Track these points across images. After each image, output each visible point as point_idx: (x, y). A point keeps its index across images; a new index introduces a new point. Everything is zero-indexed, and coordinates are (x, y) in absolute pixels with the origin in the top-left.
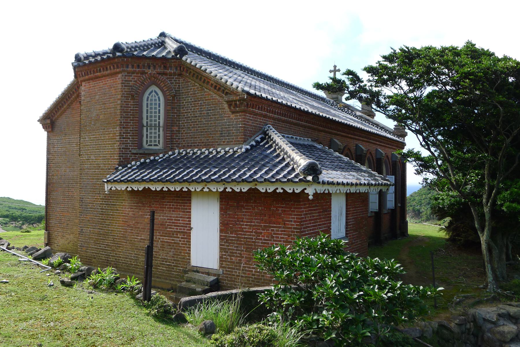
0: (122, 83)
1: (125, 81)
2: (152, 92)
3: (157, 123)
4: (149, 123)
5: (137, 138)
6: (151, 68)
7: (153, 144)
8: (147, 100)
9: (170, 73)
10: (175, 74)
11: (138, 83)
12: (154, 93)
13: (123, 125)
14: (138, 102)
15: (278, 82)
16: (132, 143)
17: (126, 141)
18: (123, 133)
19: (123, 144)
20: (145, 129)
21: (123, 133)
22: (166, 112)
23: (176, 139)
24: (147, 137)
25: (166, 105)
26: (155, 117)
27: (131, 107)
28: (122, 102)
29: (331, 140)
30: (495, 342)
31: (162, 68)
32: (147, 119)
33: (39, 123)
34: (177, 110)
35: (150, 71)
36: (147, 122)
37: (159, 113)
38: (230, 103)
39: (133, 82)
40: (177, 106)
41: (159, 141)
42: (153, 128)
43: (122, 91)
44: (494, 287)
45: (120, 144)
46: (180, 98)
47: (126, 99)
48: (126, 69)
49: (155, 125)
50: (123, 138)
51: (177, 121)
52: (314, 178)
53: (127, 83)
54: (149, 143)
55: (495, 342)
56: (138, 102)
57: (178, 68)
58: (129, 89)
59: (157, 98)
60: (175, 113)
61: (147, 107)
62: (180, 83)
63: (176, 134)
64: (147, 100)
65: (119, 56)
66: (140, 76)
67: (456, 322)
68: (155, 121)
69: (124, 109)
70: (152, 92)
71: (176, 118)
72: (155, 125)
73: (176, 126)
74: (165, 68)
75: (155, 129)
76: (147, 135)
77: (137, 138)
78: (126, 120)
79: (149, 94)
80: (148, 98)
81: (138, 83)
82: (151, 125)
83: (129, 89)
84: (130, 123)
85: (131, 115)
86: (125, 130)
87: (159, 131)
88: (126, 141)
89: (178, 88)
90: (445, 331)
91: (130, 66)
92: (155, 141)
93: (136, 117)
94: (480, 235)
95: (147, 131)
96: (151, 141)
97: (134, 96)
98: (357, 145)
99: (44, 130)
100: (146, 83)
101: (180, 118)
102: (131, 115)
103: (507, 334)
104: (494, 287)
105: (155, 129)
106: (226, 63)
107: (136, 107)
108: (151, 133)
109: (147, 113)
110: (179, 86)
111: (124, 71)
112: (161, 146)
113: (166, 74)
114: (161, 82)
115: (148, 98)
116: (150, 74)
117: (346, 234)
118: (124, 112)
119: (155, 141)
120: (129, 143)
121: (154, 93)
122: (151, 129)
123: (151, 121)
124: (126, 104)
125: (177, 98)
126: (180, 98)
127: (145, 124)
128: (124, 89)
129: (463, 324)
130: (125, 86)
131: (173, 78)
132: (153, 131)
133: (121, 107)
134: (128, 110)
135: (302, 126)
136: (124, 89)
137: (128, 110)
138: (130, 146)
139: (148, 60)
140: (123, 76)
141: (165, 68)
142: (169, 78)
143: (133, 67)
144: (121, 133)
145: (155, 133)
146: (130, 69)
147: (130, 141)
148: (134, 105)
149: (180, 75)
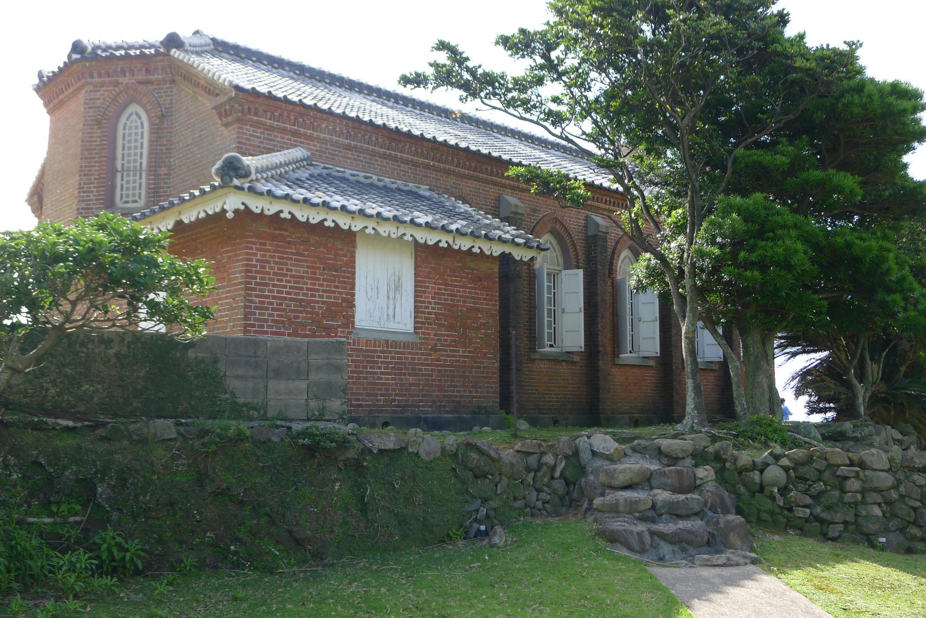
0: (85, 104)
1: (90, 99)
2: (131, 114)
3: (138, 165)
4: (126, 165)
5: (103, 191)
6: (127, 74)
7: (131, 199)
8: (124, 129)
9: (157, 80)
10: (164, 80)
11: (108, 101)
12: (134, 117)
13: (85, 171)
14: (107, 132)
15: (475, 122)
16: (97, 200)
17: (87, 196)
18: (84, 184)
19: (84, 201)
20: (119, 175)
21: (84, 184)
22: (151, 143)
23: (163, 187)
24: (122, 189)
25: (151, 132)
26: (135, 154)
27: (96, 141)
28: (83, 133)
29: (499, 197)
30: (595, 488)
31: (143, 73)
32: (123, 159)
33: (26, 203)
34: (167, 141)
35: (125, 80)
36: (123, 165)
37: (142, 148)
38: (222, 112)
39: (101, 101)
40: (168, 133)
41: (140, 194)
42: (132, 173)
43: (85, 117)
44: (693, 423)
45: (79, 201)
46: (172, 120)
47: (91, 129)
48: (90, 80)
49: (135, 167)
50: (84, 192)
51: (166, 158)
52: (224, 179)
53: (93, 103)
54: (124, 199)
55: (595, 488)
56: (107, 132)
57: (168, 71)
58: (95, 112)
59: (139, 124)
60: (165, 145)
61: (124, 139)
62: (172, 96)
63: (164, 179)
64: (124, 129)
65: (76, 59)
66: (111, 90)
67: (516, 448)
68: (135, 161)
69: (86, 146)
70: (131, 114)
71: (165, 153)
72: (135, 167)
73: (165, 166)
74: (148, 71)
75: (135, 175)
76: (122, 185)
77: (103, 191)
78: (88, 162)
79: (127, 119)
80: (125, 124)
81: (108, 101)
82: (129, 169)
83: (95, 112)
84: (95, 166)
85: (96, 154)
86: (88, 179)
87: (140, 178)
88: (87, 196)
89: (169, 104)
90: (474, 455)
91: (95, 75)
92: (134, 195)
93: (104, 157)
94: (682, 324)
95: (122, 180)
96: (127, 196)
97: (100, 123)
98: (587, 218)
99: (33, 215)
100: (121, 99)
101: (171, 153)
102: (96, 154)
103: (619, 472)
104: (693, 423)
105: (135, 175)
106: (570, 152)
107: (103, 140)
108: (128, 182)
109: (123, 149)
110: (171, 100)
111: (87, 83)
112: (142, 203)
113: (149, 82)
114: (144, 96)
115: (125, 124)
116: (127, 84)
117: (415, 328)
118: (87, 150)
119: (134, 195)
120: (92, 200)
121: (134, 117)
122: (128, 176)
123: (129, 162)
124: (90, 137)
125: (167, 120)
126: (172, 120)
127: (119, 167)
128: (88, 112)
129: (535, 453)
130: (90, 108)
131: (162, 88)
132: (131, 178)
133: (83, 141)
134: (92, 145)
135: (406, 162)
136: (88, 112)
137: (92, 145)
138: (93, 204)
139: (121, 62)
140: (86, 92)
141: (148, 71)
142: (156, 89)
143: (100, 76)
144: (80, 184)
145: (135, 181)
146: (96, 79)
147: (94, 196)
148: (101, 137)
149: (173, 81)
